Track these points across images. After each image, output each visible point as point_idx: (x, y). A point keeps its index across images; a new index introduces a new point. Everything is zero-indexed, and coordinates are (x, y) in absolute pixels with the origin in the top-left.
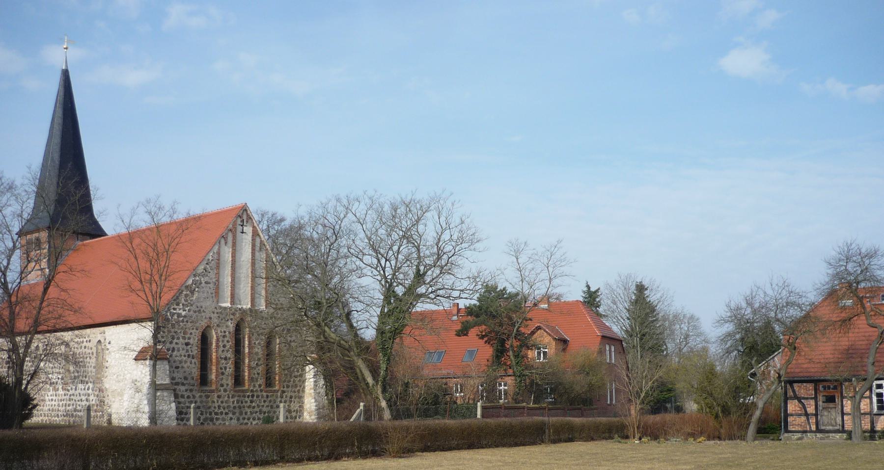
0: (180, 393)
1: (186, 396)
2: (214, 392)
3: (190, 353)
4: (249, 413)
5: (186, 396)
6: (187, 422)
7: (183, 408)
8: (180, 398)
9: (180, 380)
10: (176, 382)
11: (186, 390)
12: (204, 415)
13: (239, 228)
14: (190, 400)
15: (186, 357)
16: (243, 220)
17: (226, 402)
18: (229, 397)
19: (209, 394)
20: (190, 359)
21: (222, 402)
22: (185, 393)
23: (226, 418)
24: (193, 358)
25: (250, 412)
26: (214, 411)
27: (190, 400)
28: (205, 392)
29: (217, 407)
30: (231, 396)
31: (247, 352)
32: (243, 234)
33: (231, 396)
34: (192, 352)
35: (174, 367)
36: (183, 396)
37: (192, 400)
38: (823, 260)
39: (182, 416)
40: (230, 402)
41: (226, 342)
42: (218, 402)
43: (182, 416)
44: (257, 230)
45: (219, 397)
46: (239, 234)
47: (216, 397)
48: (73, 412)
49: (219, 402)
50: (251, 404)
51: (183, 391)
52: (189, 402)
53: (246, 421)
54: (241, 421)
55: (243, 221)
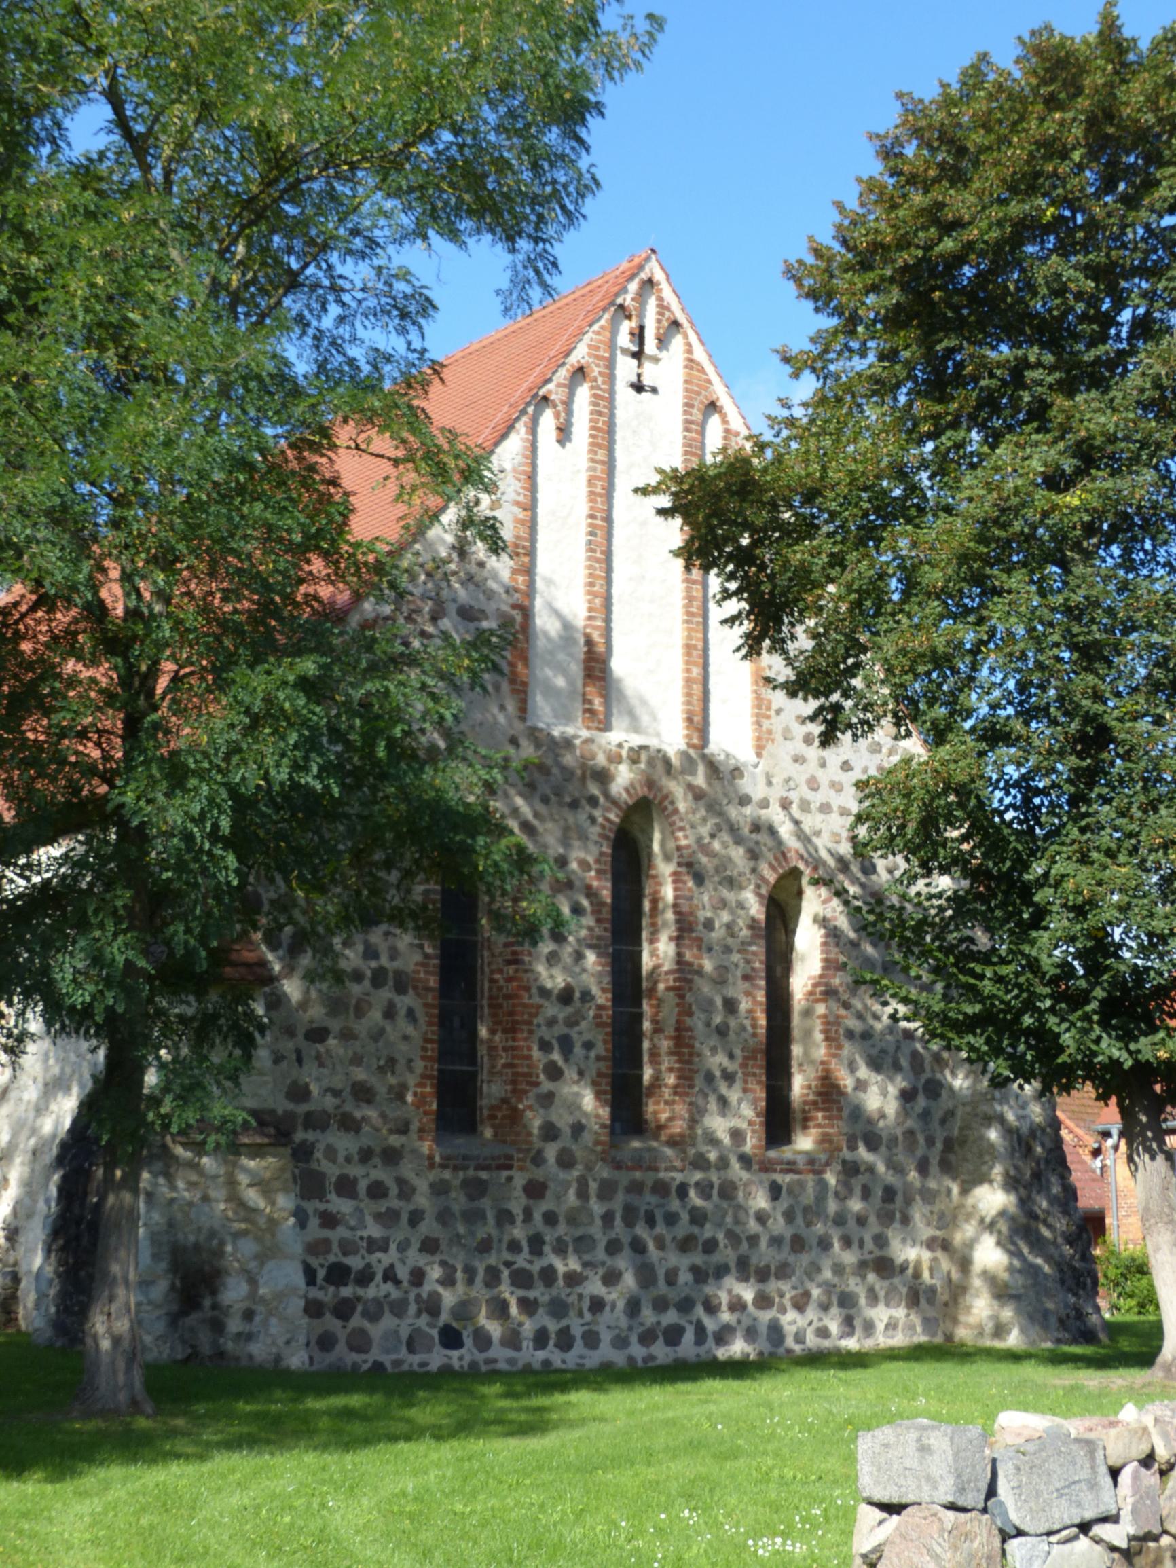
0: (332, 1171)
1: (362, 1185)
2: (510, 1167)
3: (384, 961)
4: (685, 1277)
5: (362, 1185)
6: (367, 1325)
7: (347, 1248)
8: (333, 1196)
9: (329, 1102)
10: (308, 1115)
11: (366, 1155)
12: (460, 1288)
13: (626, 368)
14: (382, 1206)
15: (367, 983)
16: (642, 328)
17: (572, 1220)
18: (583, 1194)
19: (484, 1175)
20: (386, 993)
21: (551, 1219)
22: (355, 1171)
23: (573, 1299)
24: (401, 988)
25: (694, 1269)
26: (508, 1264)
27: (382, 1206)
28: (465, 1168)
29: (524, 1244)
30: (593, 1186)
31: (1147, 1055)
32: (645, 396)
33: (593, 1186)
34: (393, 958)
35: (301, 1032)
36: (346, 1187)
37: (395, 1203)
38: (984, 746)
39: (347, 1291)
40: (591, 1215)
41: (700, 927)
42: (528, 1215)
43: (347, 1291)
44: (709, 382)
45: (535, 1190)
46: (624, 393)
47: (518, 1192)
48: (507, 143)
49: (537, 1216)
50: (696, 1230)
51: (348, 1160)
52: (378, 1217)
53: (671, 1317)
54: (648, 1315)
55: (639, 335)
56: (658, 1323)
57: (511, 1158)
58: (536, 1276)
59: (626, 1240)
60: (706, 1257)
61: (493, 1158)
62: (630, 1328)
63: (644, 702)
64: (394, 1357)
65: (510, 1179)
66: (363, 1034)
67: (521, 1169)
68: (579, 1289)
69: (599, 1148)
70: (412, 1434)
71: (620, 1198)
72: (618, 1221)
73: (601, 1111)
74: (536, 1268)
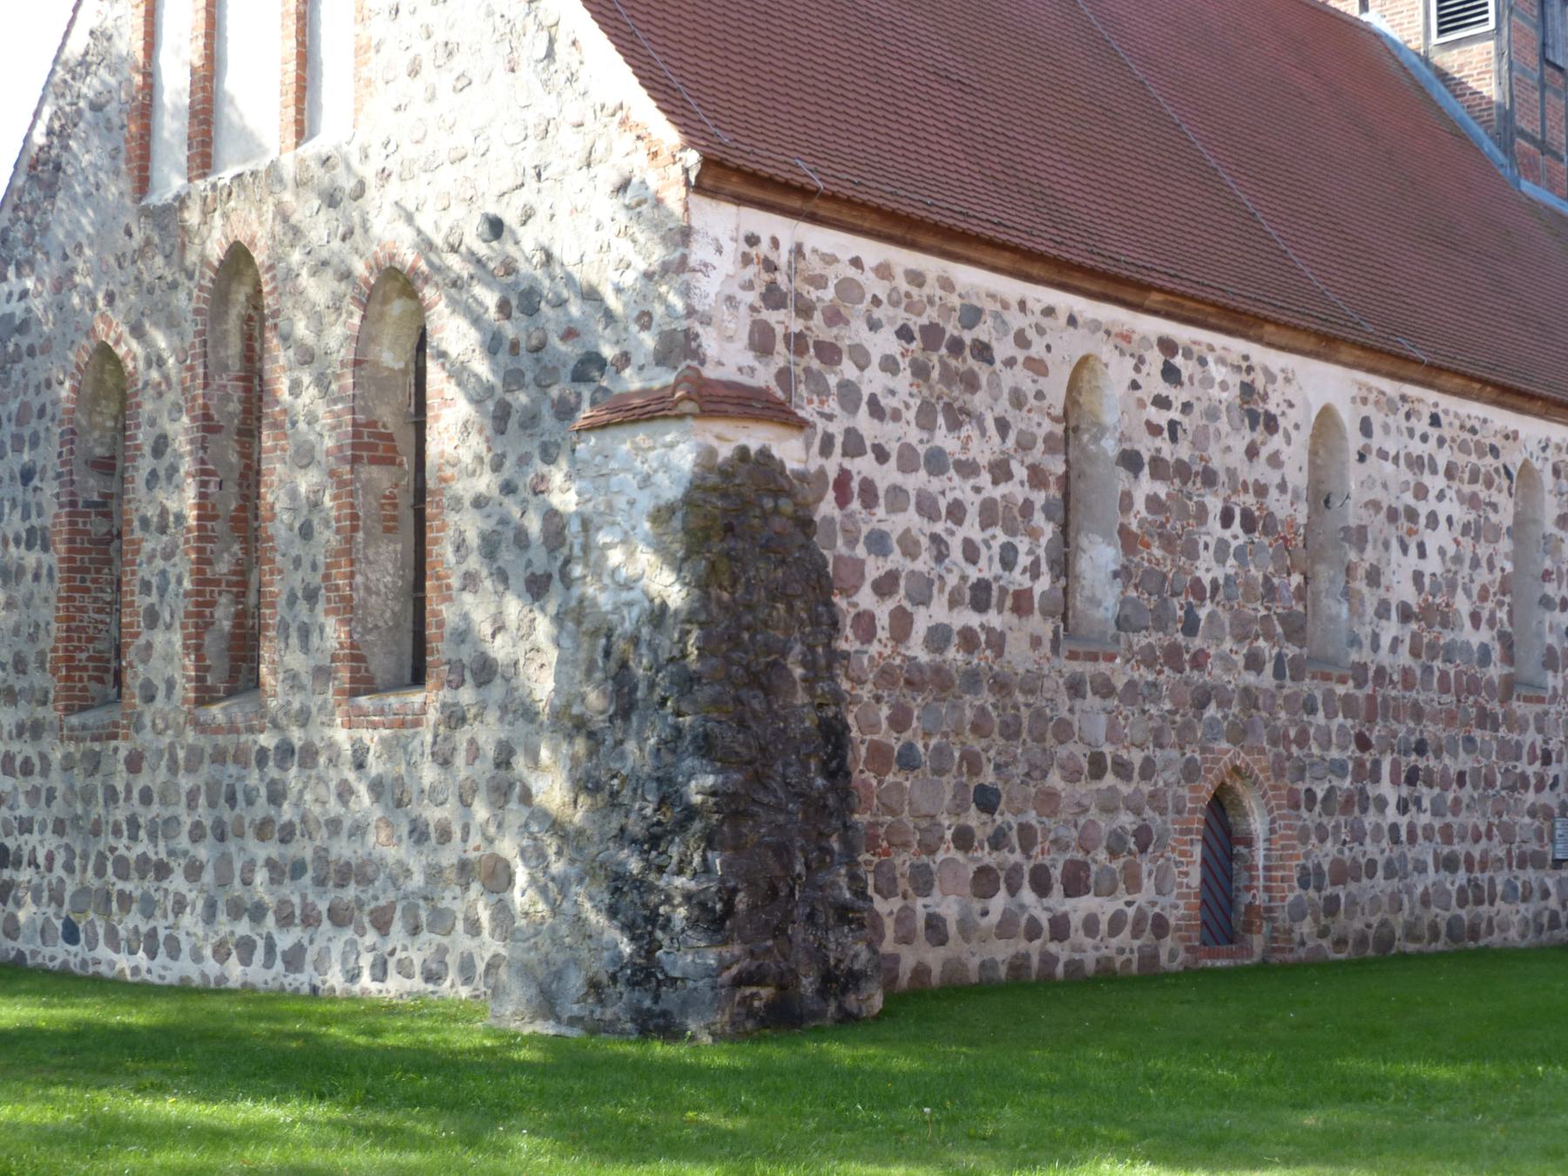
2: (114, 736)
23: (158, 896)
28: (83, 740)
56: (232, 933)
57: (116, 724)
58: (133, 865)
59: (208, 823)
60: (282, 848)
61: (103, 727)
62: (206, 938)
63: (232, 101)
64: (32, 947)
65: (116, 750)
66: (891, 604)
67: (126, 737)
68: (165, 884)
69: (185, 708)
70: (1338, 362)
71: (206, 769)
72: (202, 800)
73: (627, 624)
74: (132, 855)
